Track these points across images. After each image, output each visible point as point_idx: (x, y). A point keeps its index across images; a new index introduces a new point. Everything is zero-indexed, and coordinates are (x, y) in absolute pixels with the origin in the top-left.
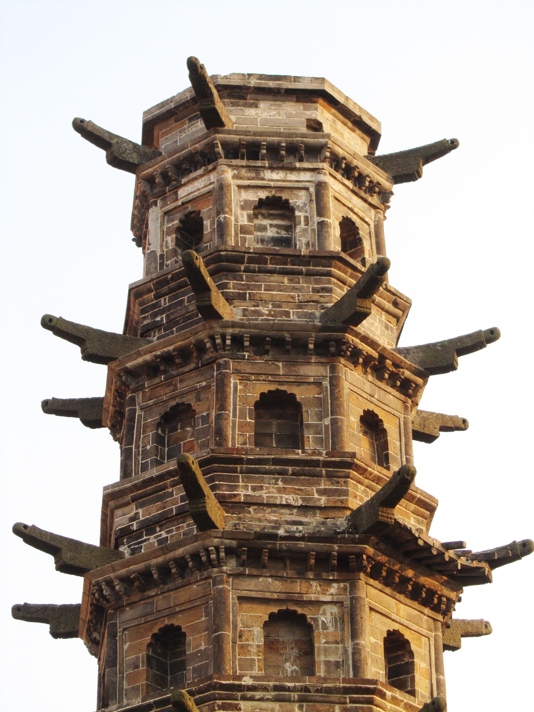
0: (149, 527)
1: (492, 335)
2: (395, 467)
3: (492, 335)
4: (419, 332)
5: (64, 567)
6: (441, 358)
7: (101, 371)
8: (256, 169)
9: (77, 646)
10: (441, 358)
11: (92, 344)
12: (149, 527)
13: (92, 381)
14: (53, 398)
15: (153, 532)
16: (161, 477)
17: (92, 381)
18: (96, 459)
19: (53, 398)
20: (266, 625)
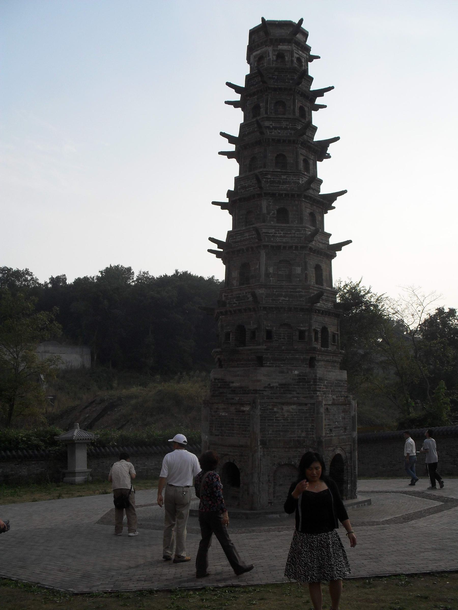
0: (275, 128)
1: (333, 88)
2: (307, 120)
3: (333, 88)
4: (314, 87)
5: (230, 142)
6: (320, 93)
7: (240, 95)
8: (298, 49)
9: (234, 160)
10: (320, 93)
11: (237, 89)
12: (275, 128)
13: (237, 97)
14: (323, 96)
15: (276, 130)
16: (281, 118)
17: (237, 97)
18: (238, 116)
19: (323, 96)
20: (276, 157)
